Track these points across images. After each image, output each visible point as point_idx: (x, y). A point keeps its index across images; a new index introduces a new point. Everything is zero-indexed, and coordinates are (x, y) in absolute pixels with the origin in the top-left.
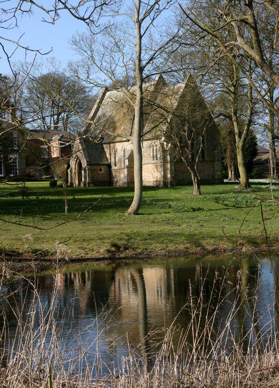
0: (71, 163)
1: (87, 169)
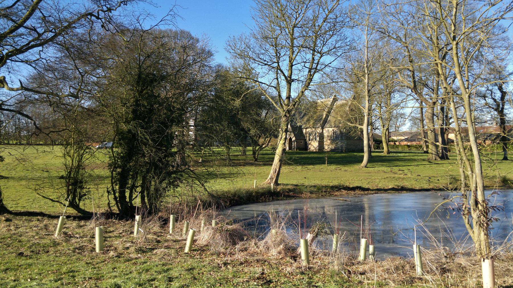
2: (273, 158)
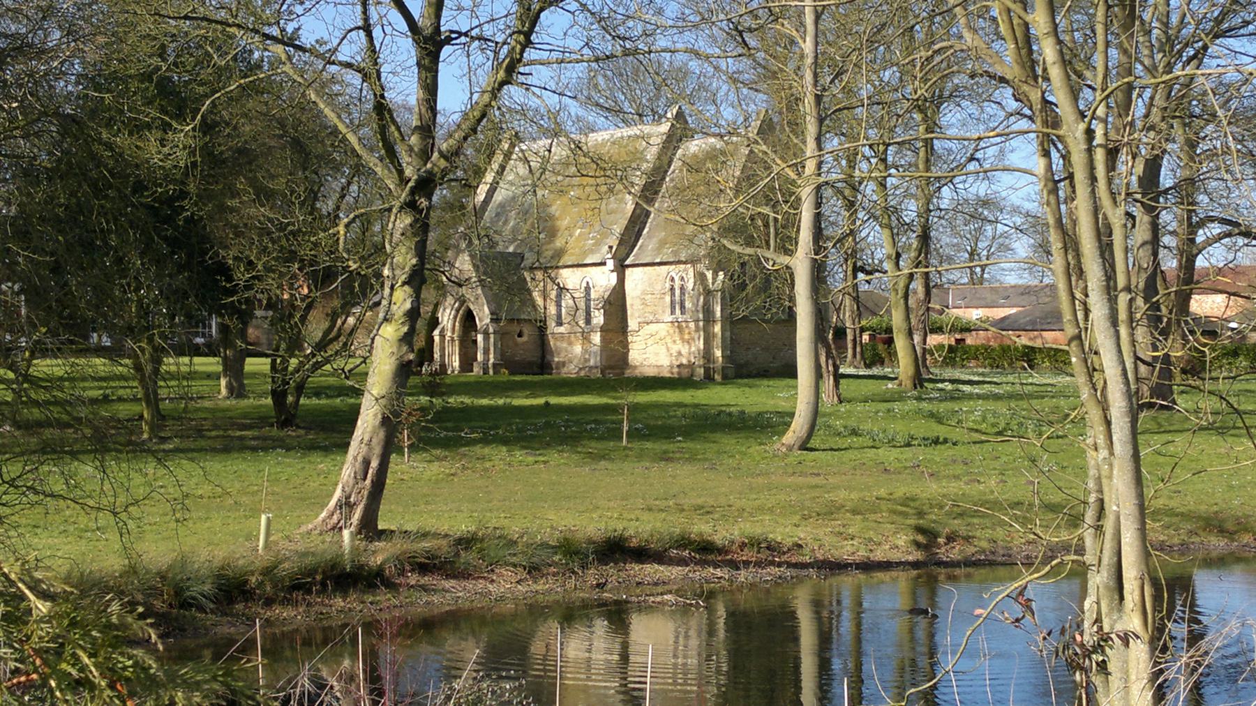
0: (440, 315)
1: (491, 330)
2: (355, 413)
